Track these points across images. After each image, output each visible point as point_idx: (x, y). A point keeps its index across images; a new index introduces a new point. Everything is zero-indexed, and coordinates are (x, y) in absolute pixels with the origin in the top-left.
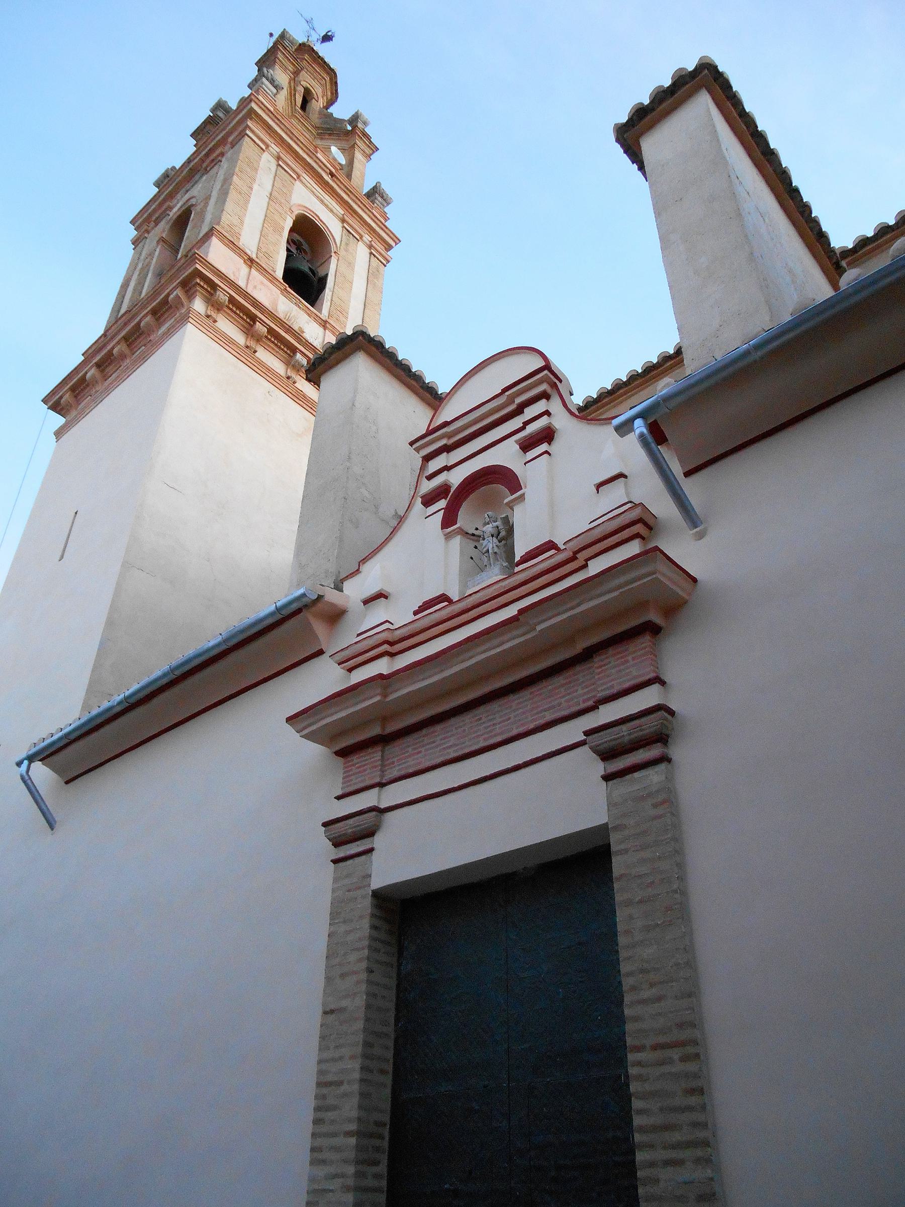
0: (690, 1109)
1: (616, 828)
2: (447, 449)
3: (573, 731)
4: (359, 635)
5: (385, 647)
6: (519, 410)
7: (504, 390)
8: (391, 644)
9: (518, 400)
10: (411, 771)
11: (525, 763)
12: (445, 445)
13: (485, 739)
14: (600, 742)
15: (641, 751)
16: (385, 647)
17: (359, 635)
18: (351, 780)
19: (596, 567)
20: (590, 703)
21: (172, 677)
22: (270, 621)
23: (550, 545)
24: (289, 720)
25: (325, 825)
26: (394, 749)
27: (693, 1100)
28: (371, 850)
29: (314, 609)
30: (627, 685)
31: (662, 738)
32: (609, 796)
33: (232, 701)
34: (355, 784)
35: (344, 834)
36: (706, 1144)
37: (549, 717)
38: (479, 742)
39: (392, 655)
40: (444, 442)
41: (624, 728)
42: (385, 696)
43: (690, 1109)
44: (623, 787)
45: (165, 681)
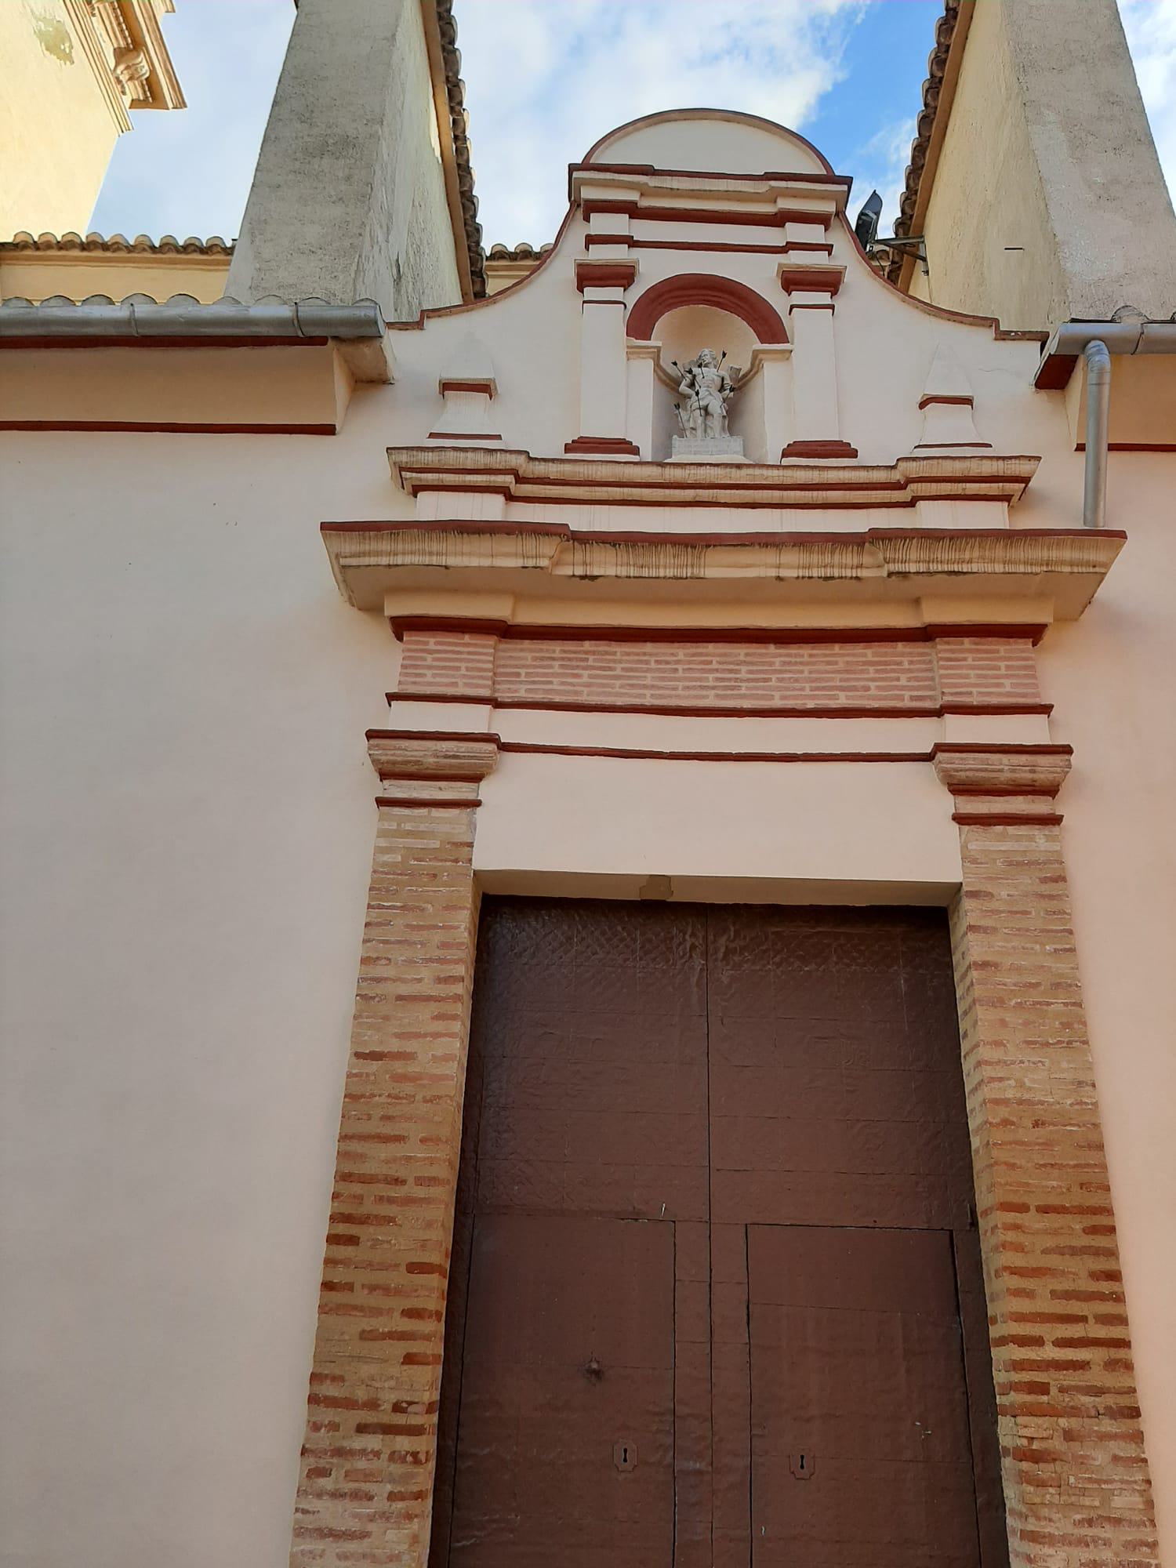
0: (1101, 1297)
1: (974, 894)
2: (633, 211)
3: (919, 735)
4: (432, 435)
5: (508, 480)
6: (778, 220)
7: (769, 177)
8: (520, 480)
9: (785, 204)
10: (557, 699)
11: (804, 755)
12: (635, 203)
13: (783, 698)
14: (963, 766)
15: (1021, 798)
16: (508, 480)
17: (432, 435)
18: (424, 675)
19: (933, 516)
20: (936, 705)
21: (124, 331)
22: (264, 331)
23: (843, 450)
24: (325, 527)
25: (371, 735)
26: (525, 652)
27: (1105, 1287)
28: (477, 804)
29: (348, 349)
30: (994, 700)
31: (1050, 791)
32: (964, 847)
33: (1164, 455)
34: (678, 696)
35: (417, 762)
36: (1125, 1344)
37: (842, 701)
38: (772, 697)
39: (510, 497)
40: (633, 196)
41: (1006, 759)
42: (557, 564)
43: (1101, 1297)
44: (983, 840)
45: (112, 331)
